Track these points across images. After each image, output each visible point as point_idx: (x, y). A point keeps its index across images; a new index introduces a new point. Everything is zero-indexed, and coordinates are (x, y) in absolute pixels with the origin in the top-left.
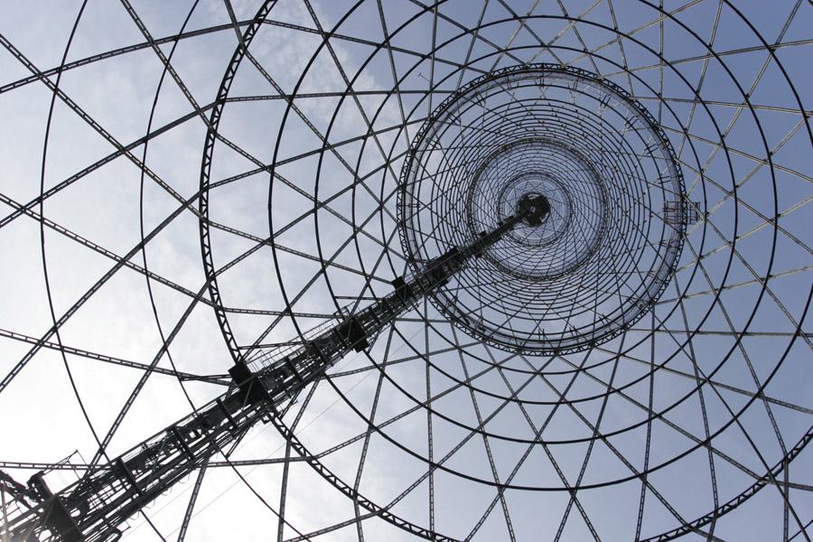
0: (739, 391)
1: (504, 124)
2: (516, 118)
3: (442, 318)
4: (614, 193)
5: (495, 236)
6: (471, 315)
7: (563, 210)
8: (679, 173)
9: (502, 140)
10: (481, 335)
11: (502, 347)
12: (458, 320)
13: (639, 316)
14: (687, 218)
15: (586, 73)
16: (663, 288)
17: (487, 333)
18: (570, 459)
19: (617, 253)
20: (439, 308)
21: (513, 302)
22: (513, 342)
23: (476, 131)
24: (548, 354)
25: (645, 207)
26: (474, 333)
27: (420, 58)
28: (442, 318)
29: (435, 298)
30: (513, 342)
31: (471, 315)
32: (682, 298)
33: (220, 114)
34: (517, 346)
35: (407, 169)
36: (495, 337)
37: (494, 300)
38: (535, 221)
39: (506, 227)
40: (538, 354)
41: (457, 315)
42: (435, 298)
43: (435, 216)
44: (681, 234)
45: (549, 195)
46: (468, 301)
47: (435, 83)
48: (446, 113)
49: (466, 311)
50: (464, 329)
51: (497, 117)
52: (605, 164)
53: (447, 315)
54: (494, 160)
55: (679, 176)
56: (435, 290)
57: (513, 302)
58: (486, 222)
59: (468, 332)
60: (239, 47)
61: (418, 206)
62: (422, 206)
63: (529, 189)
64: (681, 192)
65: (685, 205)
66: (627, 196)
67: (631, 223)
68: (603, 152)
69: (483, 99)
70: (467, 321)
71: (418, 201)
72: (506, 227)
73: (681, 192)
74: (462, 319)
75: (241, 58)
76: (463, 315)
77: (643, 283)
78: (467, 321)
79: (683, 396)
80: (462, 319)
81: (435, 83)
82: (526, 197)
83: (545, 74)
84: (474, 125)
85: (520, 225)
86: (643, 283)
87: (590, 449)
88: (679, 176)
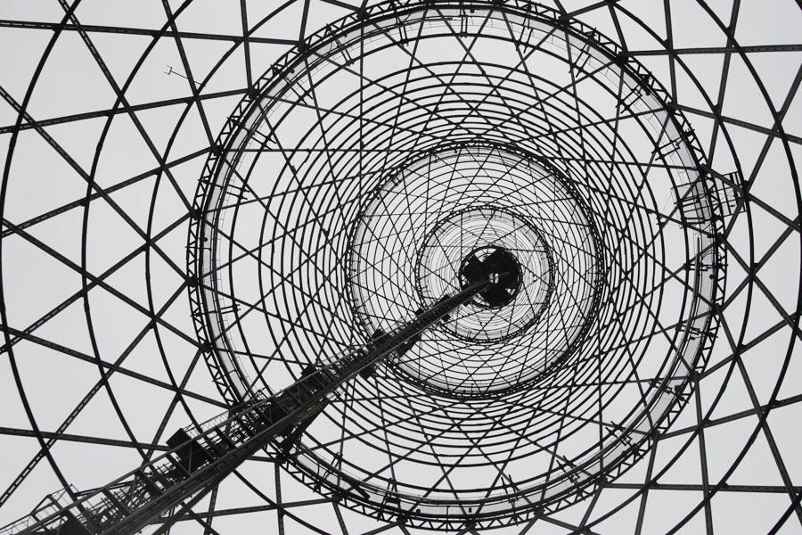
3: (317, 496)
5: (409, 334)
6: (374, 481)
7: (450, 236)
10: (392, 511)
11: (436, 525)
12: (346, 495)
13: (676, 408)
16: (708, 344)
17: (406, 506)
20: (307, 480)
22: (455, 510)
24: (524, 517)
26: (380, 510)
27: (150, 39)
28: (317, 496)
29: (296, 463)
30: (455, 510)
31: (374, 481)
34: (465, 516)
35: (197, 247)
36: (424, 509)
37: (372, 427)
38: (498, 299)
39: (436, 314)
40: (505, 521)
41: (345, 485)
42: (296, 463)
43: (275, 322)
44: (720, 239)
45: (509, 244)
46: (363, 458)
47: (199, 79)
48: (243, 133)
49: (360, 476)
50: (360, 508)
53: (324, 490)
54: (376, 202)
56: (293, 451)
58: (390, 311)
59: (369, 511)
61: (235, 310)
62: (243, 309)
63: (470, 241)
64: (697, 161)
68: (476, 109)
69: (307, 93)
70: (362, 492)
71: (234, 300)
72: (436, 314)
73: (697, 161)
74: (354, 492)
76: (355, 483)
77: (231, 239)
78: (362, 492)
80: (354, 492)
81: (199, 79)
82: (471, 258)
85: (465, 309)
86: (231, 239)
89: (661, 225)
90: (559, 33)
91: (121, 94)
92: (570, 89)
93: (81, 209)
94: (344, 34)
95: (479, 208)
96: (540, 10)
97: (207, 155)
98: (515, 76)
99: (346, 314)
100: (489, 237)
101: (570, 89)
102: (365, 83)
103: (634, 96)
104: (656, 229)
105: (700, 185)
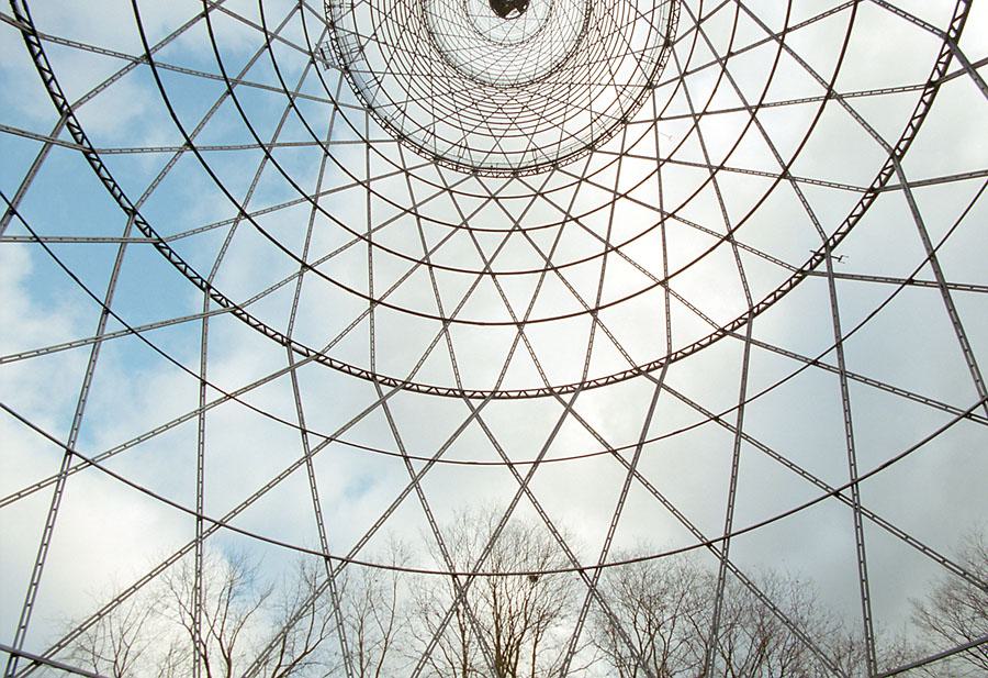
0: (95, 240)
1: (566, 96)
2: (554, 107)
4: (424, 48)
8: (360, 97)
9: (565, 76)
14: (334, 48)
15: (490, 175)
18: (705, 211)
19: (434, 82)
21: (613, 45)
23: (596, 82)
25: (385, 43)
32: (313, 58)
33: (936, 67)
47: (653, 131)
51: (575, 103)
52: (444, 79)
54: (569, 50)
55: (359, 92)
57: (613, 45)
60: (900, 157)
63: (521, 21)
64: (351, 76)
65: (342, 61)
66: (410, 50)
67: (394, 18)
73: (351, 76)
75: (899, 144)
79: (237, 528)
83: (533, 163)
84: (601, 88)
87: (600, 238)
88: (359, 92)
89: (375, 34)
90: (440, 154)
91: (782, 44)
92: (639, 15)
93: (580, 220)
94: (602, 135)
95: (511, 45)
96: (450, 166)
97: (562, 169)
98: (471, 128)
99: (407, 44)
100: (508, 25)
101: (639, 15)
102: (588, 108)
103: (395, 117)
104: (379, 32)
105: (348, 61)
